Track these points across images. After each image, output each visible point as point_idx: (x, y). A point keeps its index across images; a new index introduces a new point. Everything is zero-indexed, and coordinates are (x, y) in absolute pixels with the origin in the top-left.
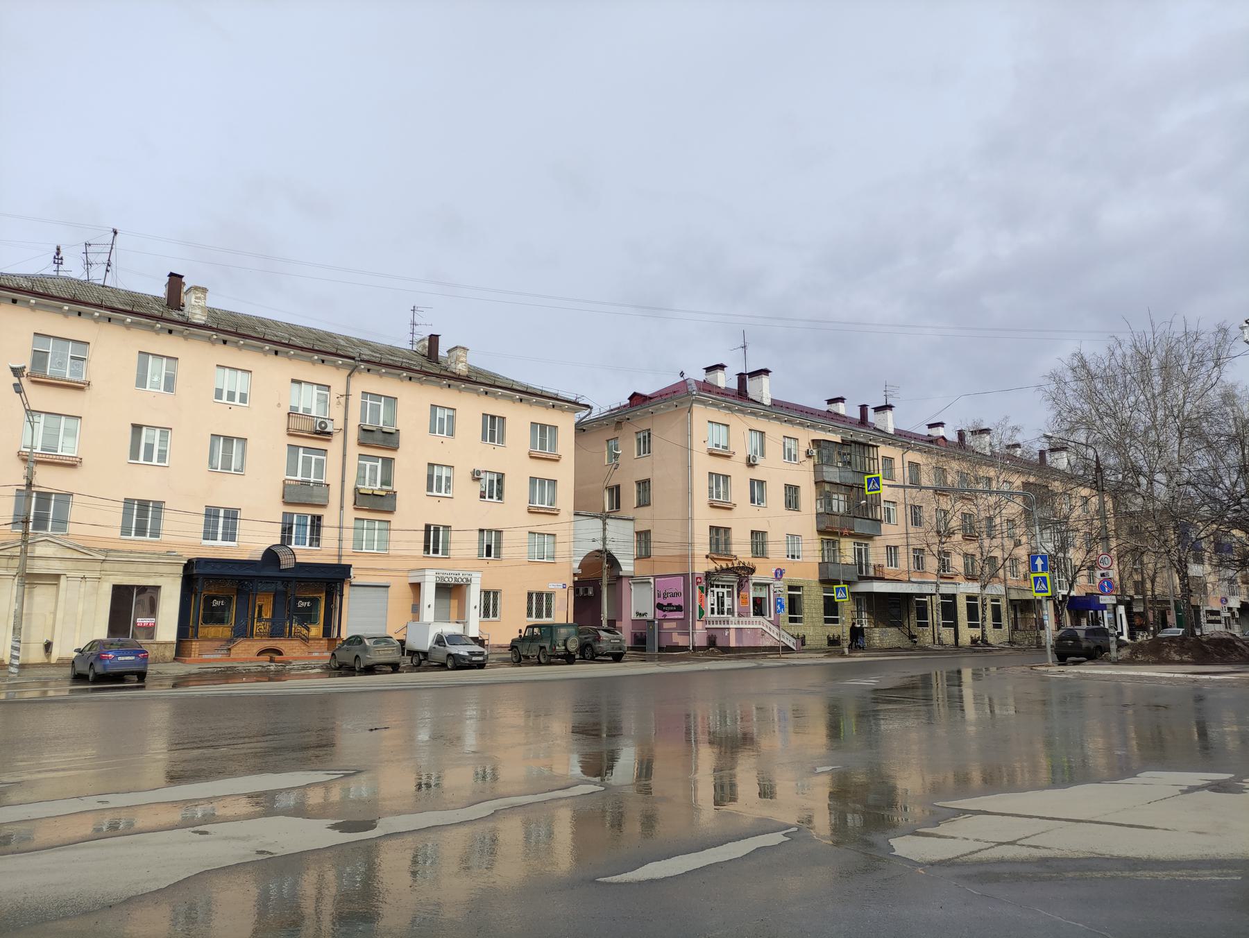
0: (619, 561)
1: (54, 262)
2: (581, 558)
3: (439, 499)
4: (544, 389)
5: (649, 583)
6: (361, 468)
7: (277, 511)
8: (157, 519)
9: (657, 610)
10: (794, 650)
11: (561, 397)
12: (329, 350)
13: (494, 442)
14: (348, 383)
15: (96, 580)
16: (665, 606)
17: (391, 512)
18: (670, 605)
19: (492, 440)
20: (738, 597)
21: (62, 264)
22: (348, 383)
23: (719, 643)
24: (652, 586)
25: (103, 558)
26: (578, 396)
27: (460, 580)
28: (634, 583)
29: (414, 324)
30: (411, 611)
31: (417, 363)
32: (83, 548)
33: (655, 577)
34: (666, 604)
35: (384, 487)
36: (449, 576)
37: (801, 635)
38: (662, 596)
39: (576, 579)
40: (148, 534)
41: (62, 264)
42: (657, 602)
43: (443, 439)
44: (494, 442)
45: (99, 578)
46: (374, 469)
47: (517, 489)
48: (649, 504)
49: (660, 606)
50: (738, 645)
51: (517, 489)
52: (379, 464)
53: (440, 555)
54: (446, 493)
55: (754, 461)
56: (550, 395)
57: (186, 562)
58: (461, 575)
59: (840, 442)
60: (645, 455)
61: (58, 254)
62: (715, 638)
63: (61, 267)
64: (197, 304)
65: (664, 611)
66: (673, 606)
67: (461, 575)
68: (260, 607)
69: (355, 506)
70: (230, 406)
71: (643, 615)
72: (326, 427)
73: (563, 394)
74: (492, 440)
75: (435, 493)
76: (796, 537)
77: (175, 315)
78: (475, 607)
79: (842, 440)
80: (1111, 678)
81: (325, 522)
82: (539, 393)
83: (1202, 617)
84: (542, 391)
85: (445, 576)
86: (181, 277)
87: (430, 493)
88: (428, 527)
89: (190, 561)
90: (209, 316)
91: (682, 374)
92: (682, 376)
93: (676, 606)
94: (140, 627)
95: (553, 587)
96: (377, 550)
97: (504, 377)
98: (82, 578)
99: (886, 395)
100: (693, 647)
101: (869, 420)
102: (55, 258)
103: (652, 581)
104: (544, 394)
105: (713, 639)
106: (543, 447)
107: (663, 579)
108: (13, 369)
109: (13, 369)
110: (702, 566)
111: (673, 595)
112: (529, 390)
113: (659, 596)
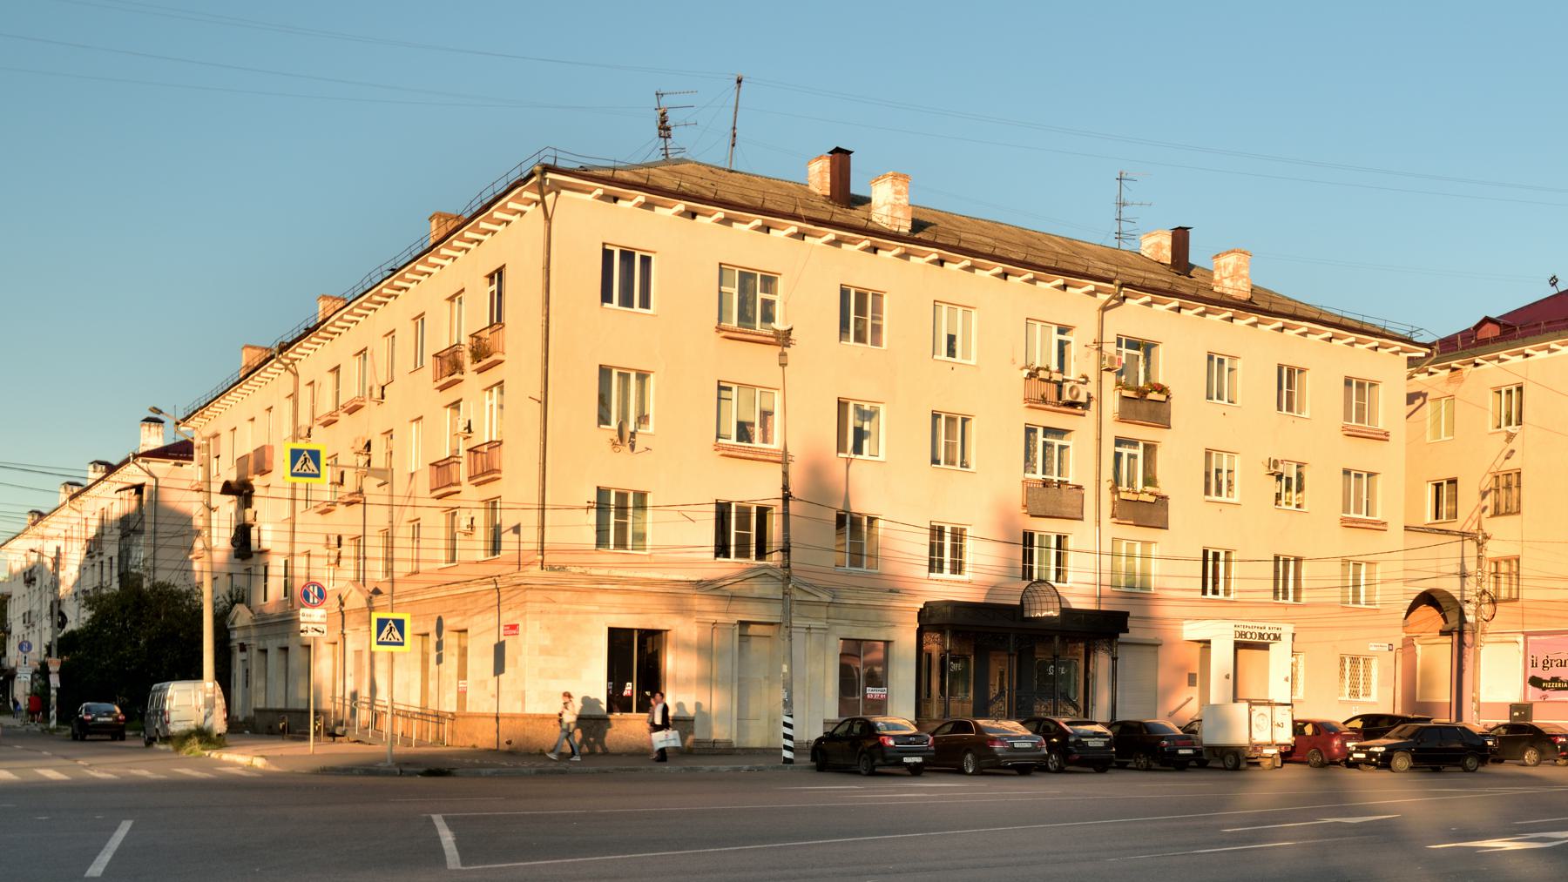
1: (660, 136)
2: (1411, 601)
4: (1345, 315)
6: (1118, 456)
8: (957, 551)
10: (318, 588)
11: (1390, 332)
13: (631, 305)
15: (822, 631)
16: (1546, 681)
18: (1555, 680)
21: (669, 137)
25: (829, 600)
26: (1414, 329)
27: (1266, 637)
28: (1120, 587)
29: (1121, 204)
31: (1165, 279)
32: (805, 584)
33: (1526, 634)
35: (1149, 489)
36: (1251, 630)
37: (545, 570)
38: (1540, 665)
39: (190, 455)
41: (669, 137)
42: (1530, 675)
43: (1225, 410)
44: (631, 305)
45: (825, 629)
47: (1323, 490)
48: (1519, 512)
50: (1404, 715)
51: (1323, 490)
52: (1139, 452)
53: (1221, 595)
54: (1228, 496)
56: (1351, 324)
57: (922, 606)
58: (1267, 628)
61: (663, 122)
64: (898, 202)
65: (1544, 689)
66: (1561, 682)
67: (1267, 628)
68: (286, 595)
69: (1115, 520)
70: (953, 365)
72: (1078, 395)
73: (1394, 328)
76: (758, 390)
77: (1183, 284)
81: (1071, 543)
82: (1357, 326)
85: (1246, 630)
86: (849, 153)
87: (1207, 498)
89: (926, 602)
91: (1554, 281)
92: (1553, 285)
94: (870, 699)
95: (1375, 649)
97: (1284, 297)
98: (807, 628)
102: (660, 128)
103: (1521, 638)
104: (1344, 322)
106: (1360, 418)
107: (1543, 638)
113: (1534, 665)
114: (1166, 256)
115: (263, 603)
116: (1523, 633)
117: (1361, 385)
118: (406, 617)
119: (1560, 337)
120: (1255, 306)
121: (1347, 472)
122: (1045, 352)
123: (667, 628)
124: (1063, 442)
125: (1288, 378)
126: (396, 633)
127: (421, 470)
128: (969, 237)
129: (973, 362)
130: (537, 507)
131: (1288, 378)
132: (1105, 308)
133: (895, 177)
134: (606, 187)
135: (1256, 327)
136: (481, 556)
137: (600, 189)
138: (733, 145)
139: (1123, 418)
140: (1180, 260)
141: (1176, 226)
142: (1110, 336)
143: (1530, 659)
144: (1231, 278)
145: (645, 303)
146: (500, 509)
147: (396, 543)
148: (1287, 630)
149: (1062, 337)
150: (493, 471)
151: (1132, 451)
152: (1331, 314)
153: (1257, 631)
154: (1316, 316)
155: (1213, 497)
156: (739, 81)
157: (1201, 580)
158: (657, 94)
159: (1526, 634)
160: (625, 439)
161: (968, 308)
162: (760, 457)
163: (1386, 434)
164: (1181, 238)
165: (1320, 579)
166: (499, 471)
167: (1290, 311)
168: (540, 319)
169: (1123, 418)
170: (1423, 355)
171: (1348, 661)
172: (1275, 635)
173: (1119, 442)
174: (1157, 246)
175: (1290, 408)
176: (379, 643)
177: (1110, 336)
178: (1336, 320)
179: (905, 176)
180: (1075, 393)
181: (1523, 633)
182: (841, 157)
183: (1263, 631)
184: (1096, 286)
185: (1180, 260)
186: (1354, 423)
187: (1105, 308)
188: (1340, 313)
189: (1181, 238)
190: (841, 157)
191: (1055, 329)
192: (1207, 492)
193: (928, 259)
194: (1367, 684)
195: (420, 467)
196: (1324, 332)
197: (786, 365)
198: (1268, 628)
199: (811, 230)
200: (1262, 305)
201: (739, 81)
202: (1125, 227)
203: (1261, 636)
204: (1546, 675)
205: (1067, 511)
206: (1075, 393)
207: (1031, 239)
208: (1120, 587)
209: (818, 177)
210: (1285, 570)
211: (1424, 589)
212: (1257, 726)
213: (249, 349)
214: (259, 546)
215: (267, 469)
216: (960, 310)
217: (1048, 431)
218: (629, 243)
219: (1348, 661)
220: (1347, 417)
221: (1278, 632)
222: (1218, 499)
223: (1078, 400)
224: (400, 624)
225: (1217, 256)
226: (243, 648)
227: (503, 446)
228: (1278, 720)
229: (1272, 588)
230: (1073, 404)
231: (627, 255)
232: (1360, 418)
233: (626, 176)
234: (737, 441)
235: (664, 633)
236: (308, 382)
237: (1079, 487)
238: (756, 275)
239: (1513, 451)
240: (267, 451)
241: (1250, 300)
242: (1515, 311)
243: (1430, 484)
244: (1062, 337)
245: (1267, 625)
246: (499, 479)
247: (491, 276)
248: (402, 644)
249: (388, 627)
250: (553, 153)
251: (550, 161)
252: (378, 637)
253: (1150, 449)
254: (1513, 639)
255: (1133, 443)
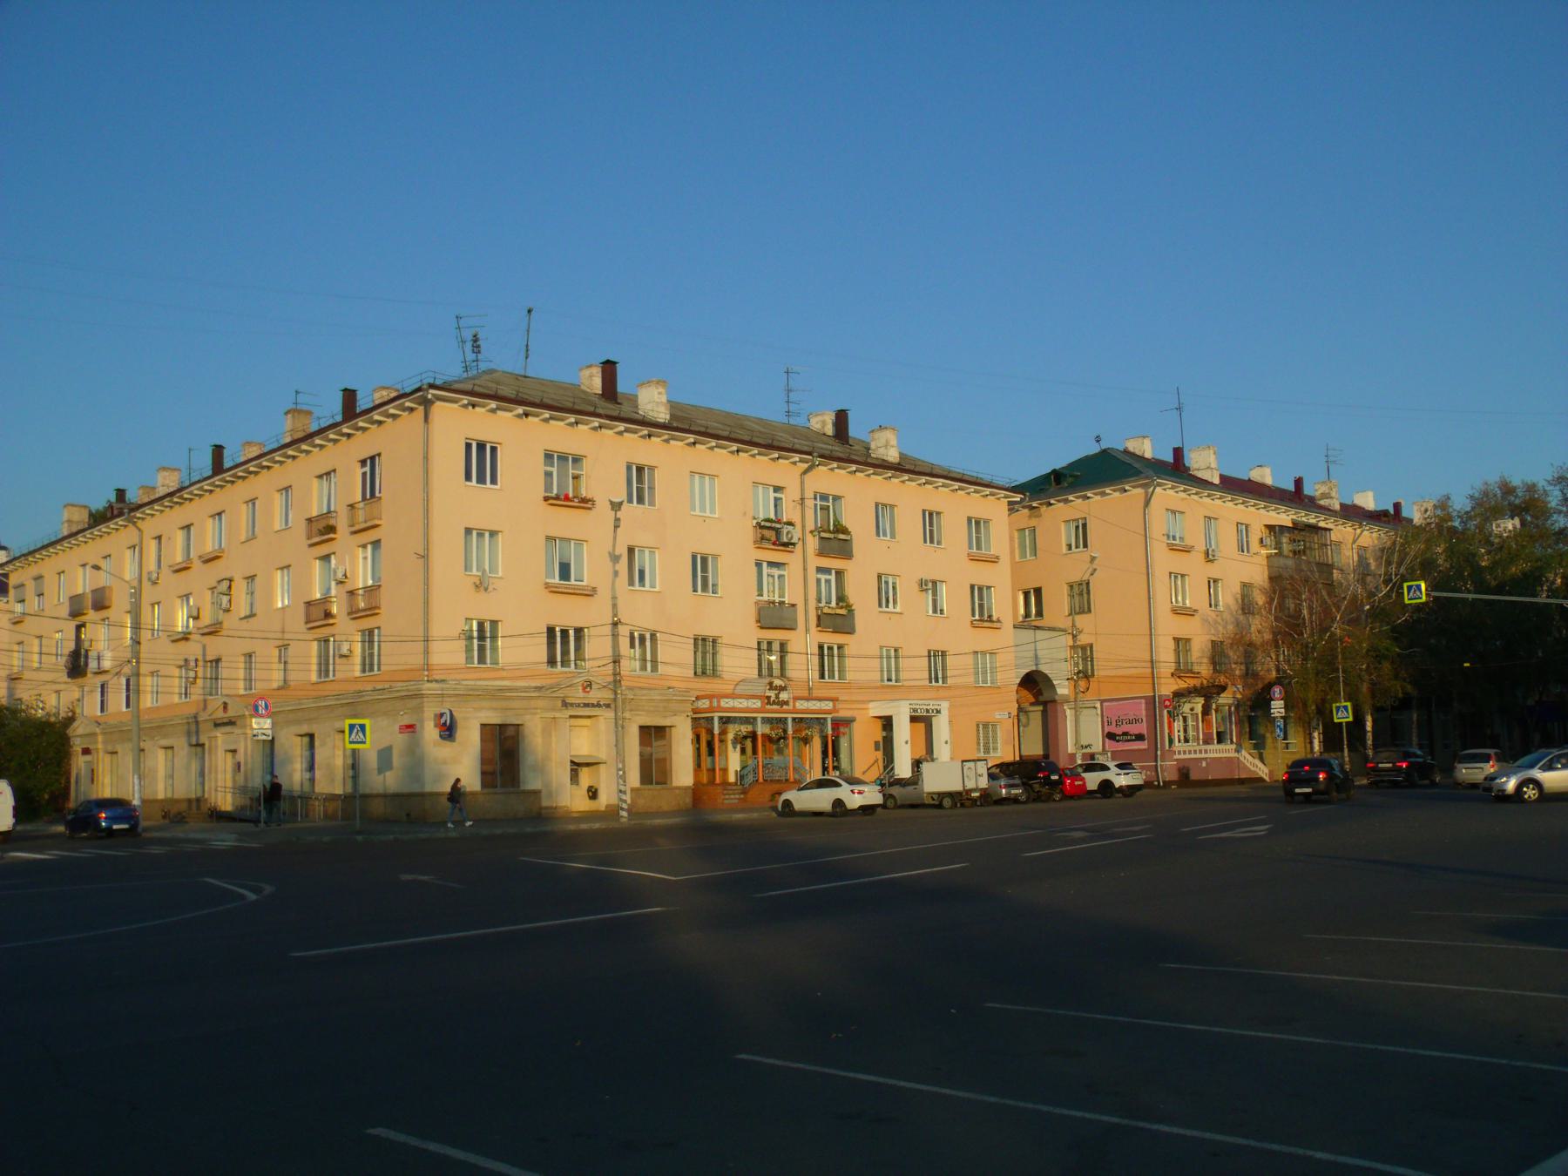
0: (1055, 682)
3: (890, 615)
4: (965, 472)
5: (1095, 708)
6: (818, 581)
7: (753, 634)
9: (1107, 740)
12: (741, 437)
13: (485, 483)
14: (802, 483)
16: (1118, 735)
17: (850, 631)
18: (1125, 734)
19: (932, 541)
20: (1203, 721)
21: (479, 352)
22: (802, 483)
23: (1194, 776)
24: (1099, 712)
30: (380, 748)
33: (1102, 701)
34: (1121, 733)
38: (1114, 724)
40: (559, 664)
41: (479, 352)
42: (1106, 732)
44: (485, 483)
46: (828, 581)
49: (1111, 736)
51: (954, 599)
52: (833, 577)
55: (1214, 556)
56: (971, 479)
59: (1291, 525)
60: (1078, 550)
62: (1188, 770)
63: (480, 357)
65: (1118, 741)
69: (819, 629)
71: (1086, 747)
72: (792, 538)
74: (640, 500)
75: (884, 609)
78: (907, 742)
79: (1293, 523)
80: (826, 888)
83: (1371, 738)
84: (707, 428)
85: (918, 707)
87: (881, 609)
88: (551, 631)
90: (900, 458)
93: (1136, 735)
95: (999, 717)
96: (491, 664)
99: (1327, 462)
100: (742, 793)
101: (1306, 493)
102: (473, 346)
103: (1098, 705)
104: (966, 478)
105: (1185, 771)
106: (979, 548)
108: (612, 503)
109: (612, 503)
110: (1168, 687)
111: (1131, 722)
112: (951, 475)
114: (830, 430)
115: (99, 714)
116: (1099, 700)
117: (978, 523)
118: (366, 722)
119: (1111, 485)
120: (904, 468)
121: (468, 531)
122: (766, 507)
123: (669, 724)
124: (782, 573)
125: (930, 517)
126: (361, 734)
127: (287, 606)
128: (714, 426)
129: (716, 516)
130: (422, 639)
131: (930, 517)
132: (805, 472)
133: (658, 383)
134: (470, 398)
135: (669, 443)
136: (358, 674)
137: (465, 400)
138: (527, 358)
139: (821, 553)
140: (610, 389)
141: (840, 409)
142: (809, 494)
143: (1105, 719)
144: (888, 447)
145: (494, 481)
146: (283, 632)
147: (141, 660)
148: (944, 706)
149: (778, 495)
150: (376, 608)
151: (828, 577)
152: (955, 472)
153: (925, 707)
154: (945, 473)
155: (884, 609)
156: (529, 311)
157: (927, 672)
158: (457, 317)
159: (1102, 701)
160: (481, 586)
161: (712, 476)
162: (578, 592)
163: (997, 557)
164: (841, 419)
165: (959, 668)
166: (379, 608)
167: (928, 471)
168: (1145, 586)
169: (821, 553)
170: (1019, 499)
171: (981, 726)
172: (936, 710)
173: (820, 570)
174: (824, 423)
175: (932, 542)
176: (351, 742)
177: (809, 494)
178: (959, 477)
179: (664, 382)
180: (790, 536)
181: (1099, 700)
182: (609, 368)
183: (928, 708)
184: (497, 405)
185: (610, 389)
186: (975, 550)
187: (805, 472)
188: (962, 471)
189: (841, 419)
190: (609, 368)
191: (771, 489)
192: (880, 605)
193: (488, 408)
194: (995, 741)
195: (286, 602)
196: (952, 485)
197: (619, 526)
198: (932, 705)
199: (606, 424)
200: (907, 467)
201: (529, 311)
202: (793, 407)
203: (928, 711)
204: (1118, 731)
205: (787, 625)
206: (790, 536)
207: (737, 421)
208: (635, 671)
209: (596, 384)
210: (936, 657)
211: (1027, 671)
212: (968, 777)
213: (70, 507)
214: (99, 668)
215: (107, 604)
216: (707, 478)
217: (771, 564)
218: (482, 438)
219: (981, 726)
220: (970, 548)
221: (938, 708)
222: (887, 610)
223: (792, 541)
224: (363, 727)
225: (873, 431)
226: (86, 751)
227: (381, 589)
228: (979, 772)
229: (928, 677)
230: (785, 545)
231: (481, 446)
232: (979, 548)
233: (456, 386)
234: (560, 580)
235: (667, 729)
236: (155, 536)
237: (793, 605)
238: (553, 455)
239: (1095, 570)
240: (107, 592)
241: (899, 464)
242: (1076, 461)
243: (1020, 592)
244: (778, 495)
245: (931, 703)
246: (377, 614)
247: (363, 463)
248: (364, 743)
249: (355, 730)
250: (431, 374)
251: (431, 381)
252: (350, 737)
253: (839, 574)
254: (1093, 705)
255: (827, 571)
